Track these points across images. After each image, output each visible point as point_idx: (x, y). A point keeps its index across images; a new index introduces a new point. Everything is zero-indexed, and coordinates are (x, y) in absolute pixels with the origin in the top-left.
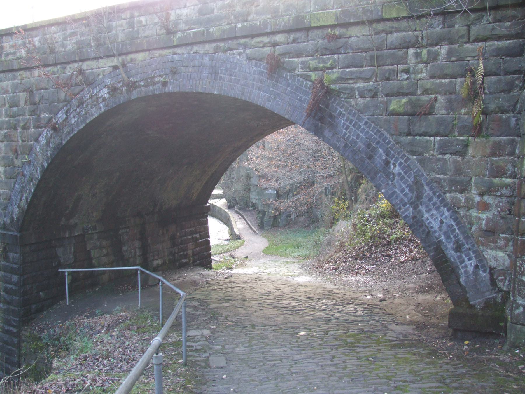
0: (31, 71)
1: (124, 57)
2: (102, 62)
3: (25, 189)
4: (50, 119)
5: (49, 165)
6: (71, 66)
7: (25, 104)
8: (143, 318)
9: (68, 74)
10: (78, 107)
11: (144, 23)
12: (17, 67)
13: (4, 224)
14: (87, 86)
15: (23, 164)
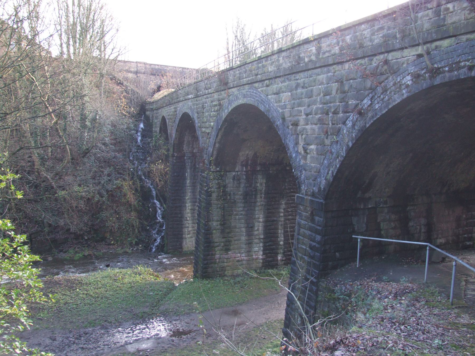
0: (342, 65)
1: (428, 45)
2: (406, 52)
3: (332, 164)
4: (357, 105)
5: (353, 145)
6: (377, 57)
7: (336, 93)
8: (430, 292)
9: (374, 65)
10: (382, 94)
11: (451, 9)
12: (331, 63)
13: (313, 192)
14: (391, 75)
15: (332, 143)
